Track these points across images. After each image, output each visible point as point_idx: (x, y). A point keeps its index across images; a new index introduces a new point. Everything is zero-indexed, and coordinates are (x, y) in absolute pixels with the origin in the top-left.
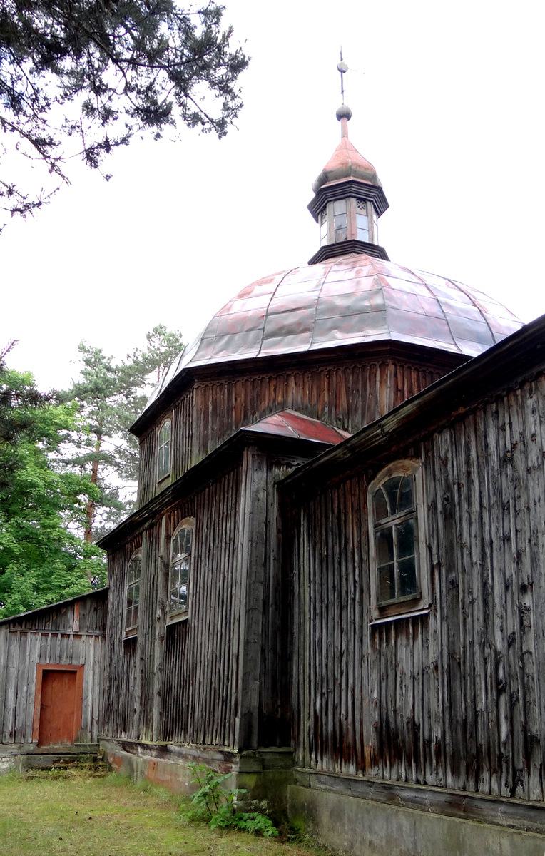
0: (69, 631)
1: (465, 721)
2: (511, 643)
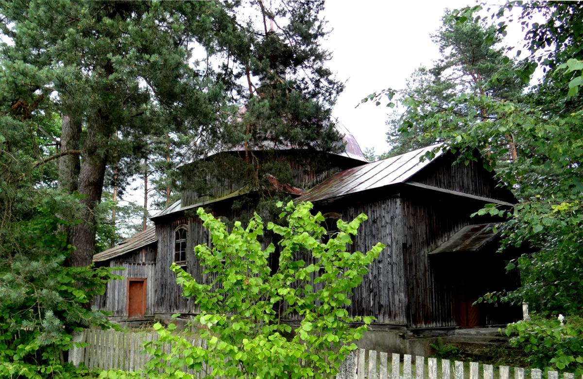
0: (140, 262)
1: (358, 301)
2: (375, 277)
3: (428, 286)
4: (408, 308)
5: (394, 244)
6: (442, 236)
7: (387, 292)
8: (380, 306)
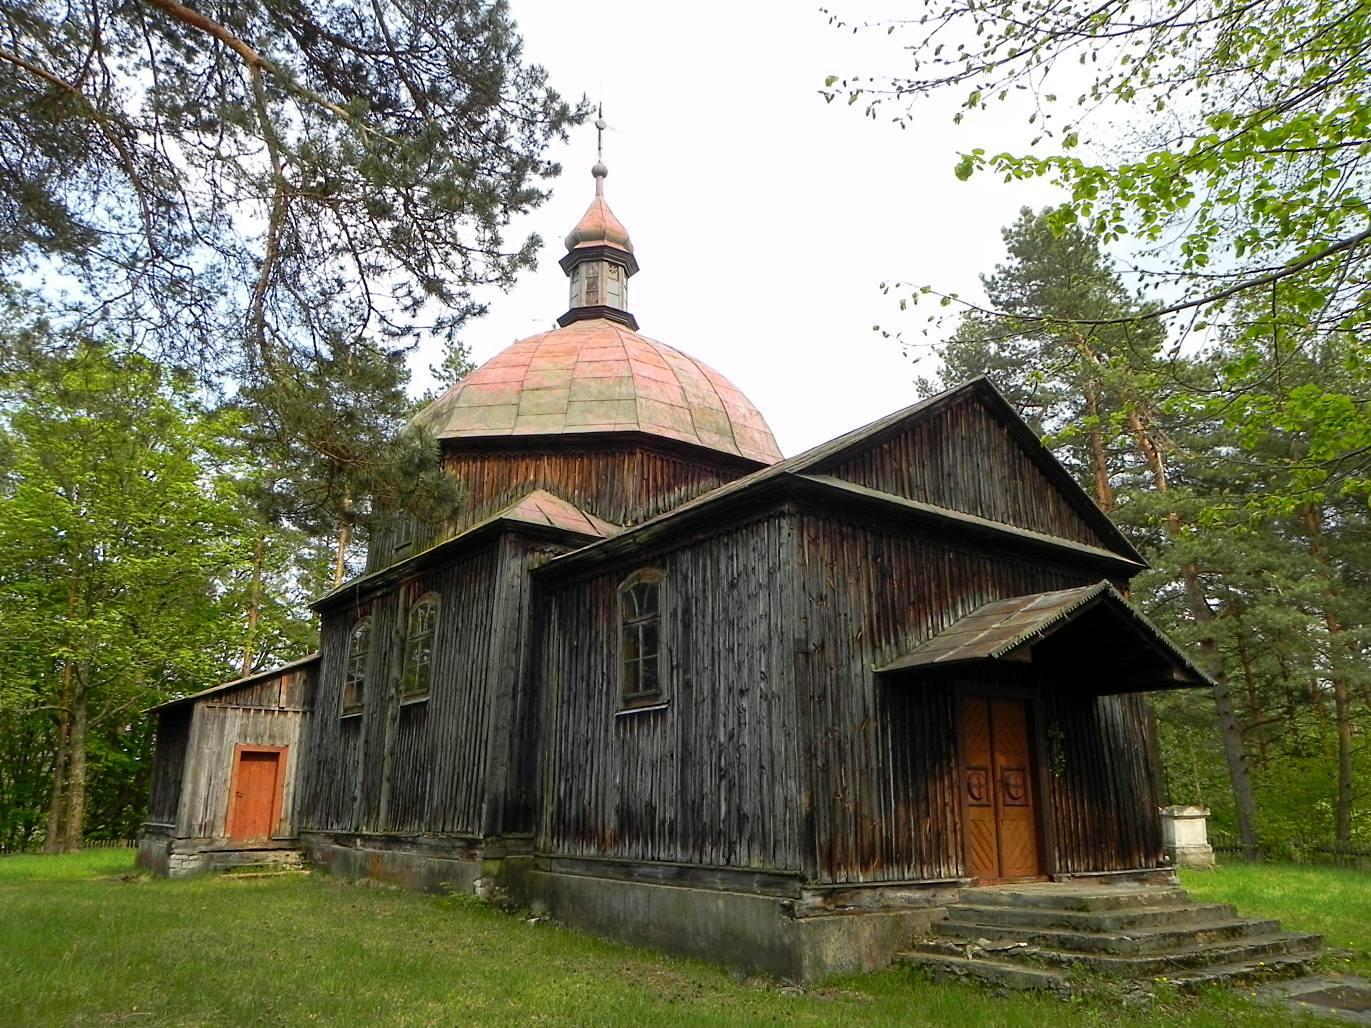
0: (274, 707)
2: (731, 737)
3: (874, 762)
4: (810, 823)
5: (775, 641)
6: (918, 625)
7: (757, 778)
8: (742, 818)
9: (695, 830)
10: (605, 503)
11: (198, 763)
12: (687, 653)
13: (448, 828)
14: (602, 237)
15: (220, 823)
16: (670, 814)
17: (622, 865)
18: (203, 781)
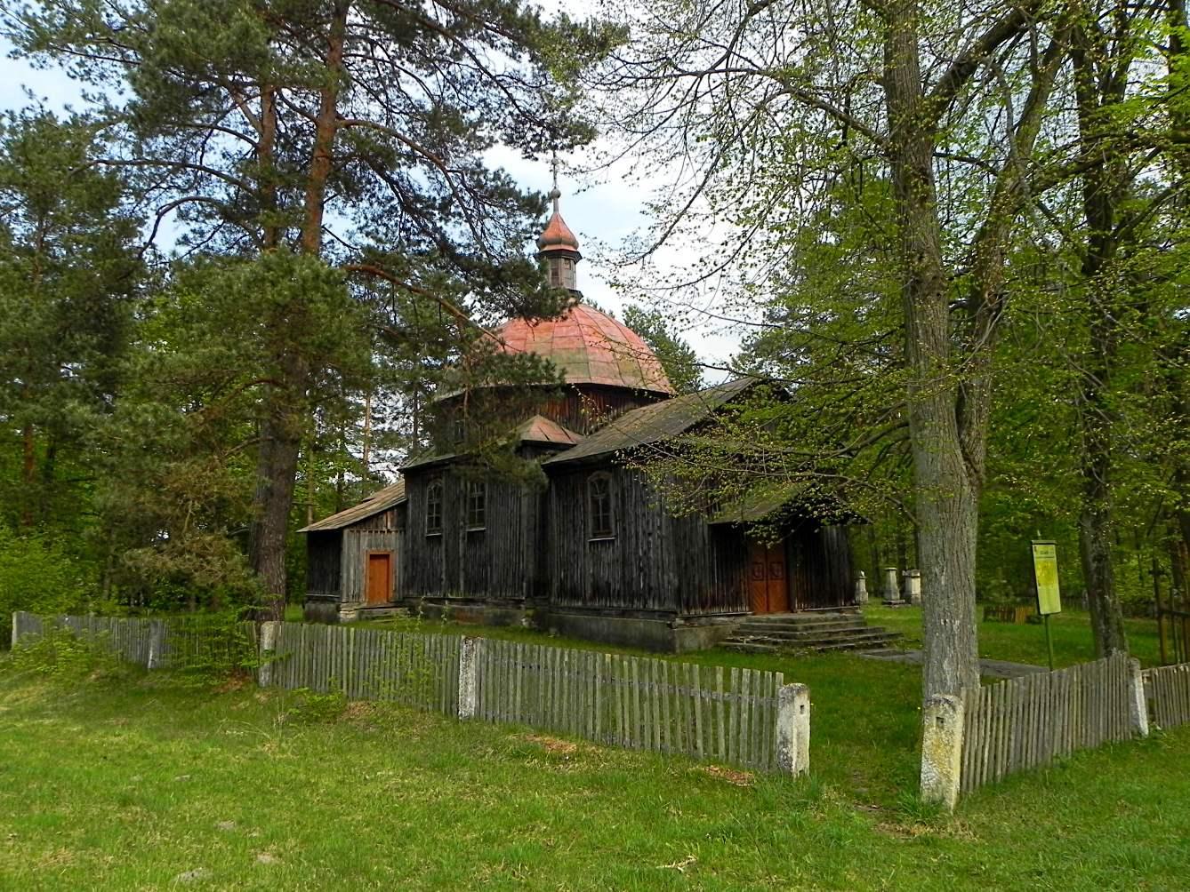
0: (384, 529)
4: (679, 590)
8: (650, 589)
9: (629, 593)
10: (574, 421)
11: (349, 562)
12: (624, 515)
13: (504, 594)
14: (559, 242)
15: (362, 594)
16: (618, 587)
17: (595, 609)
18: (352, 572)
